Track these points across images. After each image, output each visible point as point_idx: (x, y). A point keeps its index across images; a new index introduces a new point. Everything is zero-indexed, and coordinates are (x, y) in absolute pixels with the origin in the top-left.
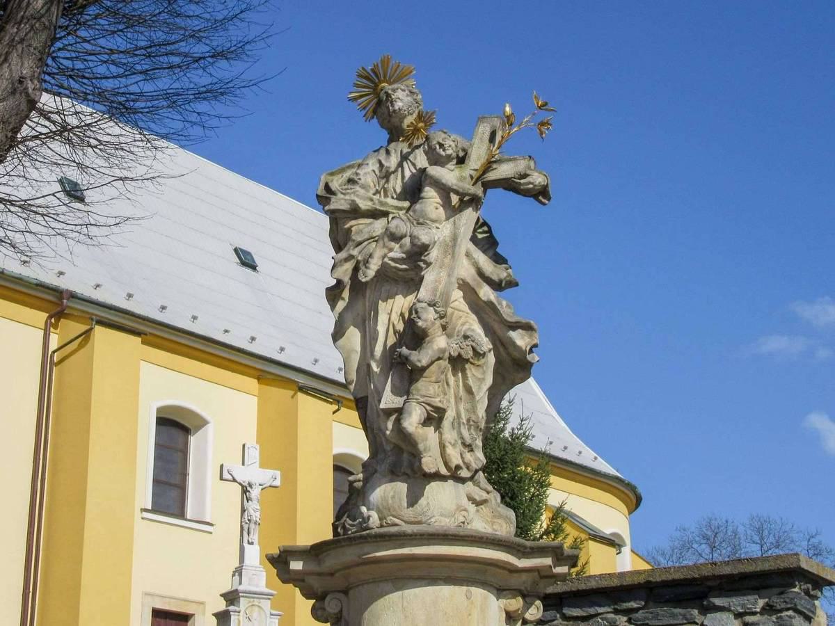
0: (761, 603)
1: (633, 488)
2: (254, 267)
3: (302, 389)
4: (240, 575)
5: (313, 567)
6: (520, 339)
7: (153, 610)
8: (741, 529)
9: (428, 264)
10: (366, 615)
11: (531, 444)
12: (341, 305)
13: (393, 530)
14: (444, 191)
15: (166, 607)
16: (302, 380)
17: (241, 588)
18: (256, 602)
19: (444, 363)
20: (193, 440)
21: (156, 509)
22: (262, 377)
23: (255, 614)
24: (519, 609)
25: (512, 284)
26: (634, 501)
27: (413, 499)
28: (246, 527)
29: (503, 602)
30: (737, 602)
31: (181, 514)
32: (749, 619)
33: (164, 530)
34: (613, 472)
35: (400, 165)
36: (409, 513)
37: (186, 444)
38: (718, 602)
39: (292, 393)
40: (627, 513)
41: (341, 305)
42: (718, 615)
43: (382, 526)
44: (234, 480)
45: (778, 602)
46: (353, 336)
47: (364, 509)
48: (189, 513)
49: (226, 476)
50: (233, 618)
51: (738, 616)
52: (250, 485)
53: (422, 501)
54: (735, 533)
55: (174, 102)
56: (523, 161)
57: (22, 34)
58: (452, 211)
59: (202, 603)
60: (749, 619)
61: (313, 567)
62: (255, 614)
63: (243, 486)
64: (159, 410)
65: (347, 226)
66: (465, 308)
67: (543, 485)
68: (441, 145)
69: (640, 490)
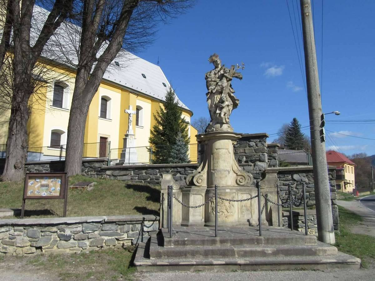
0: (259, 140)
1: (192, 112)
2: (142, 74)
3: (131, 92)
4: (129, 131)
5: (205, 137)
6: (237, 102)
7: (52, 133)
8: (207, 120)
9: (224, 90)
10: (213, 144)
11: (179, 105)
12: (208, 96)
13: (217, 132)
14: (227, 78)
15: (103, 136)
16: (129, 90)
17: (129, 134)
18: (132, 136)
19: (227, 106)
20: (108, 103)
21: (101, 117)
22: (122, 90)
23: (131, 138)
24: (233, 144)
25: (234, 92)
26: (192, 114)
27: (221, 127)
28: (130, 122)
29: (232, 142)
30: (255, 140)
31: (105, 118)
32: (257, 143)
33: (102, 121)
34: (188, 109)
35: (218, 73)
36: (220, 129)
37: (107, 103)
38: (252, 140)
39: (128, 93)
40: (190, 116)
41: (208, 96)
42: (252, 142)
43: (216, 131)
44: (128, 113)
45: (261, 140)
46: (210, 101)
47: (212, 128)
48: (107, 118)
49: (126, 112)
50: (127, 139)
51: (255, 142)
52: (131, 114)
53: (222, 127)
54: (206, 120)
55: (142, 45)
56: (81, 3)
57: (120, 33)
58: (228, 81)
59: (110, 135)
60: (257, 143)
61: (205, 137)
62: (131, 138)
63: (129, 114)
64: (102, 97)
65: (210, 83)
66: (228, 97)
67: (181, 113)
68: (227, 71)
69: (193, 113)
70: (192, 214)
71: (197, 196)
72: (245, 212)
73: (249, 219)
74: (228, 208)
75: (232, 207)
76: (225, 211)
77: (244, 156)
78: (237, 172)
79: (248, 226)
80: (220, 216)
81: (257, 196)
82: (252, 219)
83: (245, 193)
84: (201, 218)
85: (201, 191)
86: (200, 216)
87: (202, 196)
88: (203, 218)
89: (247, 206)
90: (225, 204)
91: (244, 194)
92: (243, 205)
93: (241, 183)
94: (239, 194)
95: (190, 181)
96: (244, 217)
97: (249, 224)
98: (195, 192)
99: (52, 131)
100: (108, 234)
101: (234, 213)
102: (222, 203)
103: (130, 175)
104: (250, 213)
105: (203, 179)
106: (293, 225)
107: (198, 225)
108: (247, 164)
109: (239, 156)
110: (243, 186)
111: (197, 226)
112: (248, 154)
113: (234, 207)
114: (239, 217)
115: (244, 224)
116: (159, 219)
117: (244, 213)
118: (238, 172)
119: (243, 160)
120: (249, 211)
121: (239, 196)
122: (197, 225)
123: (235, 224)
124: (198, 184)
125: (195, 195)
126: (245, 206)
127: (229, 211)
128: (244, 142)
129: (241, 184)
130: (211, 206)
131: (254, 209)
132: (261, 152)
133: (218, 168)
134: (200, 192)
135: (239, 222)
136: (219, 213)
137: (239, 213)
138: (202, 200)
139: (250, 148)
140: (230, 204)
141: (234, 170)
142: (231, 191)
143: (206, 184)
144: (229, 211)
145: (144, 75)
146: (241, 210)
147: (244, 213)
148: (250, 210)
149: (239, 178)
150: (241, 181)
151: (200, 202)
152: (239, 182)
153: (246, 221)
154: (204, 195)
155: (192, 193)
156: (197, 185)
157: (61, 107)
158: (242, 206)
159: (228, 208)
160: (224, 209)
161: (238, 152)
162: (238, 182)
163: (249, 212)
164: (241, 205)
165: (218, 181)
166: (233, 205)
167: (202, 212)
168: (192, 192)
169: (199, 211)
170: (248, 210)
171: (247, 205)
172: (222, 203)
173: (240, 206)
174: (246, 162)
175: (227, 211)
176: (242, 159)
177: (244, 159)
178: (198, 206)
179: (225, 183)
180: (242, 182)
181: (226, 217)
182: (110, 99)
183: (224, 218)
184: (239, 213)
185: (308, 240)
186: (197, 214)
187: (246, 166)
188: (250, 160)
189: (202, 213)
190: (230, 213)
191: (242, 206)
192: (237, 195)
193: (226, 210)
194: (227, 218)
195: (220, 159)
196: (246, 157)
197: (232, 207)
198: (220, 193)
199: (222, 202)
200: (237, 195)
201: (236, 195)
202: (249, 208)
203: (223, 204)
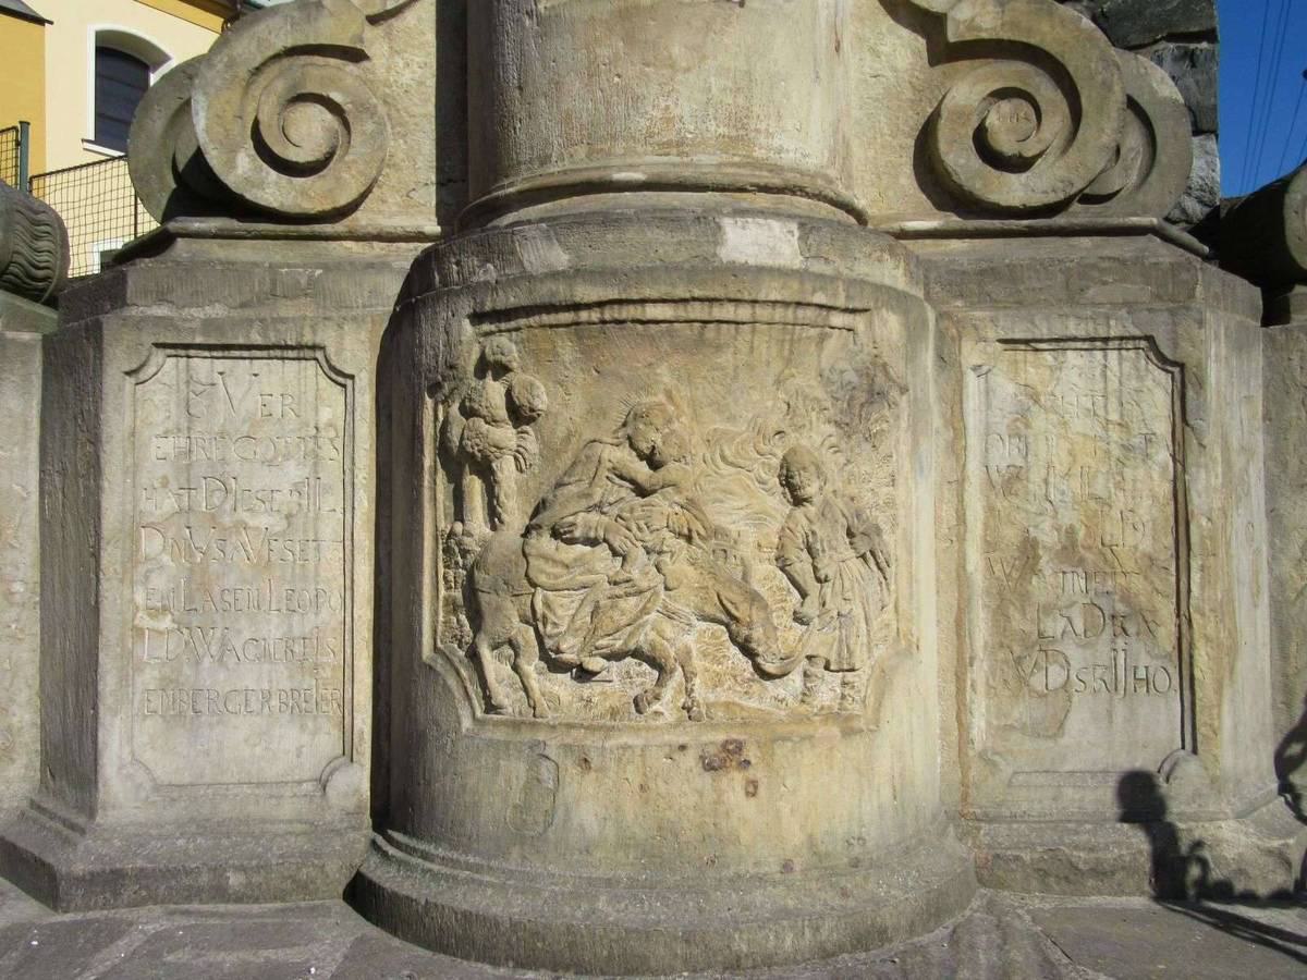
70: (149, 678)
71: (240, 368)
72: (1076, 656)
73: (1144, 761)
74: (765, 577)
75: (840, 558)
76: (692, 638)
79: (1140, 902)
80: (592, 741)
82: (1191, 768)
83: (1073, 328)
84: (327, 742)
85: (312, 290)
86: (299, 707)
87: (340, 377)
88: (348, 753)
89: (1107, 548)
90: (690, 505)
91: (1061, 342)
92: (1047, 536)
93: (1014, 180)
94: (971, 354)
95: (181, 167)
97: (1146, 864)
98: (217, 311)
101: (884, 679)
102: (642, 491)
104: (1167, 680)
105: (366, 109)
106: (420, 606)
107: (235, 880)
110: (1039, 220)
111: (220, 893)
113: (873, 557)
114: (964, 740)
115: (1061, 872)
116: (1061, 680)
120: (1149, 627)
121: (972, 383)
122: (218, 871)
123: (894, 895)
124: (274, 191)
125: (202, 366)
126: (1069, 551)
127: (790, 635)
129: (1012, 190)
130: (451, 546)
131: (1225, 610)
132: (1171, 38)
134: (286, 309)
135: (963, 815)
136: (584, 675)
137: (979, 673)
138: (331, 454)
140: (798, 501)
142: (817, 267)
143: (429, 197)
144: (781, 637)
146: (1000, 614)
147: (1056, 676)
148: (1166, 609)
149: (968, 88)
150: (1005, 144)
151: (294, 472)
152: (976, 162)
153: (1105, 797)
154: (358, 352)
155: (139, 324)
156: (252, 195)
158: (1029, 550)
159: (765, 577)
160: (685, 604)
162: (960, 160)
163: (1150, 656)
164: (1011, 535)
165: (577, 98)
166: (863, 537)
167: (333, 642)
168: (161, 311)
169: (273, 628)
170: (1123, 619)
171: (1112, 529)
172: (642, 491)
173: (990, 546)
175: (748, 651)
180: (1020, 164)
181: (725, 759)
183: (686, 787)
184: (979, 673)
186: (250, 677)
189: (331, 660)
190: (795, 680)
191: (1029, 550)
192: (946, 360)
193: (730, 620)
194: (734, 781)
197: (840, 558)
198: (586, 292)
199: (641, 470)
200: (946, 360)
201: (928, 358)
202: (1138, 584)
203: (663, 506)
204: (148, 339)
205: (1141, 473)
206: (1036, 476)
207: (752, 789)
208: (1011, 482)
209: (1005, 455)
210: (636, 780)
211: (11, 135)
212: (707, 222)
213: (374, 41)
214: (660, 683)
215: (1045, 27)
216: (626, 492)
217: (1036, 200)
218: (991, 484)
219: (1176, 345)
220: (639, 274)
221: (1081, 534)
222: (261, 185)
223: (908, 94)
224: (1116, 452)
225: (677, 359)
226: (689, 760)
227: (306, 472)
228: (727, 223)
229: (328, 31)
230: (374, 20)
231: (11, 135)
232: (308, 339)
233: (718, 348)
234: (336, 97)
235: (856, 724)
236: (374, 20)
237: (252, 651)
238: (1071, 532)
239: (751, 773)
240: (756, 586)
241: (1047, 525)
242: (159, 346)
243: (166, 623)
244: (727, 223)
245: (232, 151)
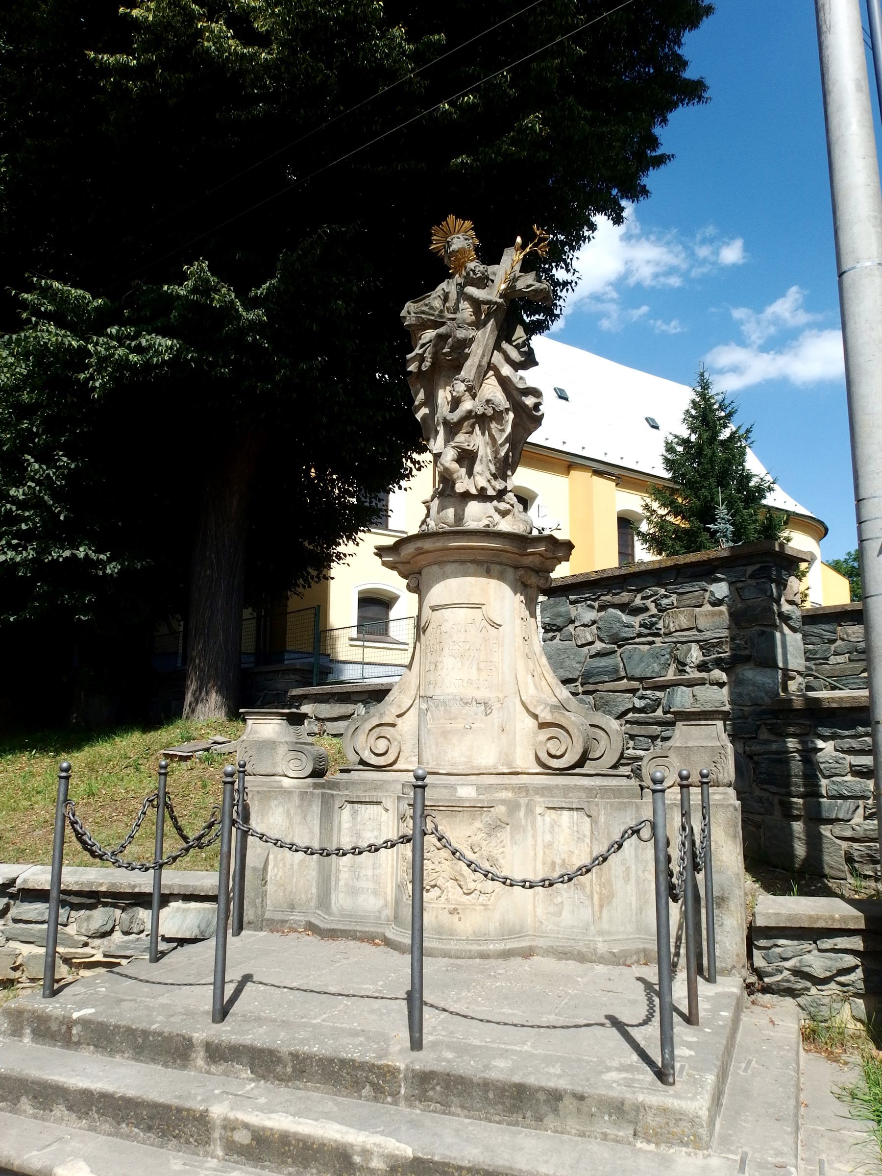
26: (824, 531)
77: (693, 645)
78: (535, 707)
81: (405, 839)
96: (560, 913)
99: (360, 592)
100: (33, 936)
103: (355, 715)
108: (704, 675)
109: (673, 645)
112: (707, 635)
117: (559, 900)
118: (542, 707)
119: (688, 661)
128: (692, 586)
133: (438, 691)
139: (716, 608)
141: (523, 698)
145: (653, 420)
147: (559, 900)
157: (386, 528)
161: (672, 625)
164: (549, 860)
174: (702, 667)
176: (686, 656)
177: (695, 655)
178: (370, 846)
179: (463, 759)
181: (454, 911)
182: (534, 496)
185: (649, 1119)
187: (704, 684)
188: (717, 658)
194: (456, 917)
195: (446, 652)
196: (701, 648)
204: (344, 800)
205: (582, 845)
206: (556, 844)
207: (460, 919)
208: (549, 845)
209: (548, 837)
210: (435, 915)
211: (313, 611)
212: (453, 787)
213: (399, 721)
214: (442, 894)
215: (563, 720)
216: (435, 848)
217: (561, 767)
218: (544, 846)
219: (590, 811)
220: (438, 800)
221: (567, 861)
222: (371, 759)
223: (532, 734)
224: (576, 839)
225: (447, 819)
226: (446, 911)
227: (378, 833)
228: (458, 787)
229: (387, 719)
230: (398, 716)
231: (313, 611)
232: (379, 800)
233: (456, 817)
234: (388, 736)
235: (489, 907)
236: (398, 716)
237: (365, 878)
238: (564, 860)
239: (460, 915)
240: (463, 872)
241: (558, 858)
242: (346, 801)
243: (346, 869)
244: (458, 787)
245: (364, 749)
